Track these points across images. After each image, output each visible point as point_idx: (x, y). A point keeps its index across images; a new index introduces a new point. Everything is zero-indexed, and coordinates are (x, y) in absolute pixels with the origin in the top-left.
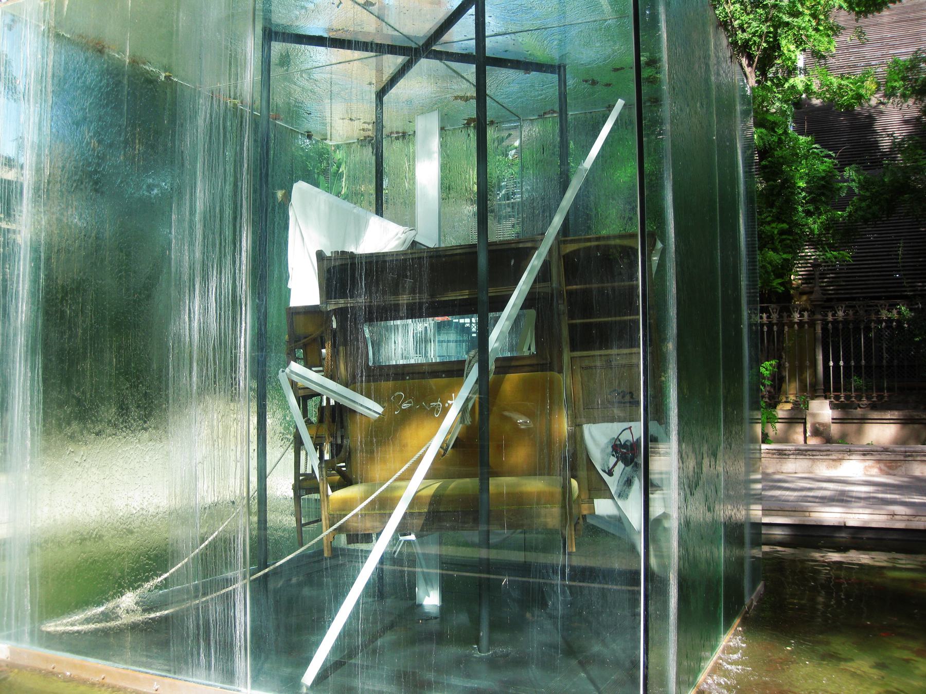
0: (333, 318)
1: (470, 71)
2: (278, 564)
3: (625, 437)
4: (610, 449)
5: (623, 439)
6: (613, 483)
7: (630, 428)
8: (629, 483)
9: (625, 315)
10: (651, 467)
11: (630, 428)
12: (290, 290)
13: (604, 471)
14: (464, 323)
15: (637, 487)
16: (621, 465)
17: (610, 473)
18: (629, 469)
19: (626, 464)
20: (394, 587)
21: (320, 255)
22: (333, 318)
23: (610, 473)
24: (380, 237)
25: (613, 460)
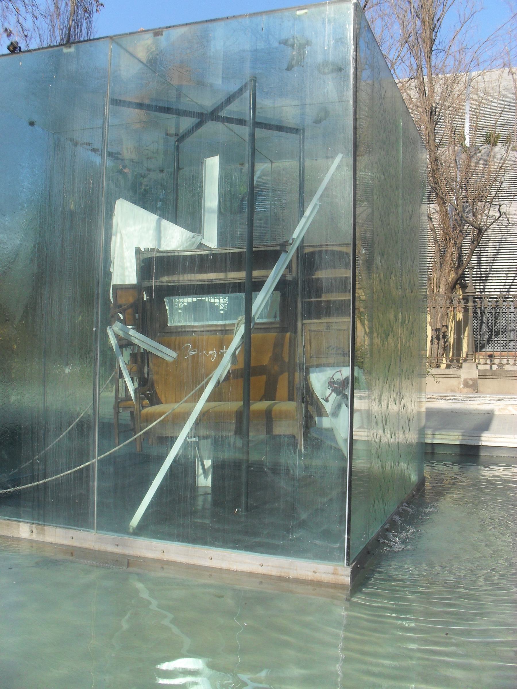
0: (144, 293)
1: (245, 131)
2: (148, 428)
3: (338, 377)
4: (327, 385)
5: (336, 378)
6: (328, 407)
7: (340, 371)
8: (339, 406)
9: (100, 342)
10: (354, 447)
11: (340, 371)
12: (111, 273)
13: (323, 399)
14: (215, 303)
15: (345, 412)
16: (334, 395)
17: (327, 401)
18: (339, 397)
19: (338, 394)
20: (183, 471)
21: (138, 251)
22: (144, 293)
23: (327, 401)
24: (175, 238)
25: (328, 392)
